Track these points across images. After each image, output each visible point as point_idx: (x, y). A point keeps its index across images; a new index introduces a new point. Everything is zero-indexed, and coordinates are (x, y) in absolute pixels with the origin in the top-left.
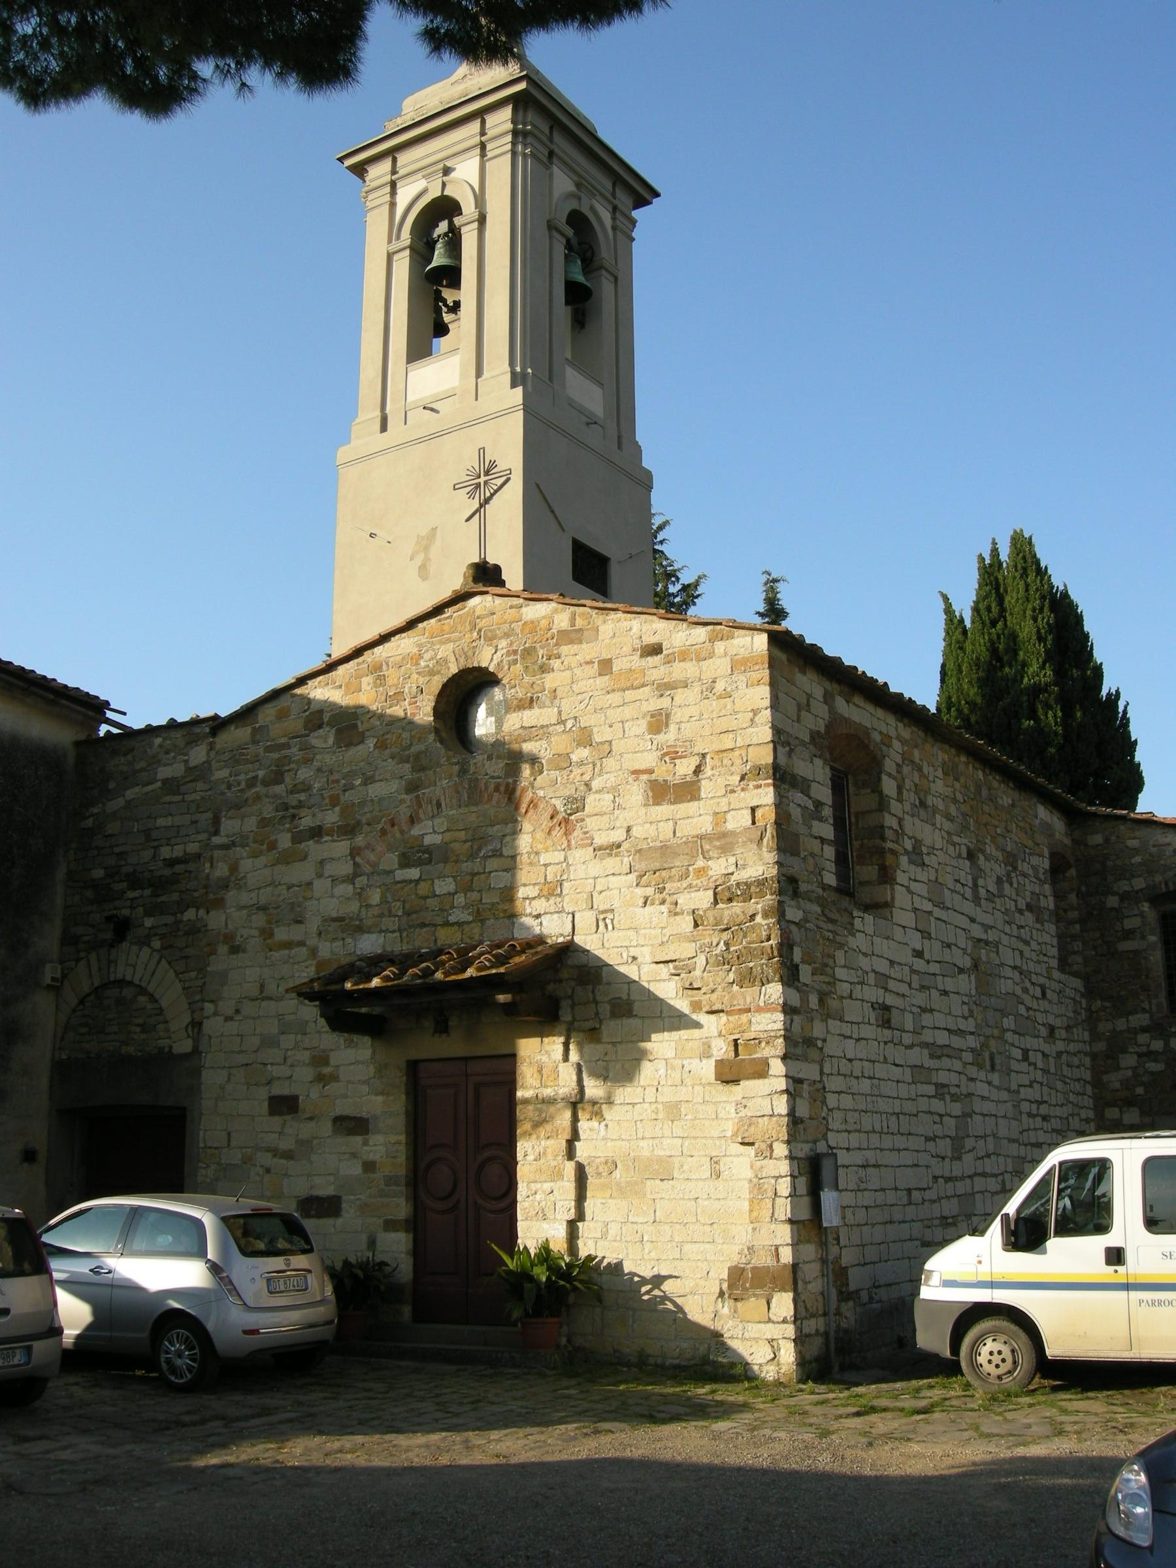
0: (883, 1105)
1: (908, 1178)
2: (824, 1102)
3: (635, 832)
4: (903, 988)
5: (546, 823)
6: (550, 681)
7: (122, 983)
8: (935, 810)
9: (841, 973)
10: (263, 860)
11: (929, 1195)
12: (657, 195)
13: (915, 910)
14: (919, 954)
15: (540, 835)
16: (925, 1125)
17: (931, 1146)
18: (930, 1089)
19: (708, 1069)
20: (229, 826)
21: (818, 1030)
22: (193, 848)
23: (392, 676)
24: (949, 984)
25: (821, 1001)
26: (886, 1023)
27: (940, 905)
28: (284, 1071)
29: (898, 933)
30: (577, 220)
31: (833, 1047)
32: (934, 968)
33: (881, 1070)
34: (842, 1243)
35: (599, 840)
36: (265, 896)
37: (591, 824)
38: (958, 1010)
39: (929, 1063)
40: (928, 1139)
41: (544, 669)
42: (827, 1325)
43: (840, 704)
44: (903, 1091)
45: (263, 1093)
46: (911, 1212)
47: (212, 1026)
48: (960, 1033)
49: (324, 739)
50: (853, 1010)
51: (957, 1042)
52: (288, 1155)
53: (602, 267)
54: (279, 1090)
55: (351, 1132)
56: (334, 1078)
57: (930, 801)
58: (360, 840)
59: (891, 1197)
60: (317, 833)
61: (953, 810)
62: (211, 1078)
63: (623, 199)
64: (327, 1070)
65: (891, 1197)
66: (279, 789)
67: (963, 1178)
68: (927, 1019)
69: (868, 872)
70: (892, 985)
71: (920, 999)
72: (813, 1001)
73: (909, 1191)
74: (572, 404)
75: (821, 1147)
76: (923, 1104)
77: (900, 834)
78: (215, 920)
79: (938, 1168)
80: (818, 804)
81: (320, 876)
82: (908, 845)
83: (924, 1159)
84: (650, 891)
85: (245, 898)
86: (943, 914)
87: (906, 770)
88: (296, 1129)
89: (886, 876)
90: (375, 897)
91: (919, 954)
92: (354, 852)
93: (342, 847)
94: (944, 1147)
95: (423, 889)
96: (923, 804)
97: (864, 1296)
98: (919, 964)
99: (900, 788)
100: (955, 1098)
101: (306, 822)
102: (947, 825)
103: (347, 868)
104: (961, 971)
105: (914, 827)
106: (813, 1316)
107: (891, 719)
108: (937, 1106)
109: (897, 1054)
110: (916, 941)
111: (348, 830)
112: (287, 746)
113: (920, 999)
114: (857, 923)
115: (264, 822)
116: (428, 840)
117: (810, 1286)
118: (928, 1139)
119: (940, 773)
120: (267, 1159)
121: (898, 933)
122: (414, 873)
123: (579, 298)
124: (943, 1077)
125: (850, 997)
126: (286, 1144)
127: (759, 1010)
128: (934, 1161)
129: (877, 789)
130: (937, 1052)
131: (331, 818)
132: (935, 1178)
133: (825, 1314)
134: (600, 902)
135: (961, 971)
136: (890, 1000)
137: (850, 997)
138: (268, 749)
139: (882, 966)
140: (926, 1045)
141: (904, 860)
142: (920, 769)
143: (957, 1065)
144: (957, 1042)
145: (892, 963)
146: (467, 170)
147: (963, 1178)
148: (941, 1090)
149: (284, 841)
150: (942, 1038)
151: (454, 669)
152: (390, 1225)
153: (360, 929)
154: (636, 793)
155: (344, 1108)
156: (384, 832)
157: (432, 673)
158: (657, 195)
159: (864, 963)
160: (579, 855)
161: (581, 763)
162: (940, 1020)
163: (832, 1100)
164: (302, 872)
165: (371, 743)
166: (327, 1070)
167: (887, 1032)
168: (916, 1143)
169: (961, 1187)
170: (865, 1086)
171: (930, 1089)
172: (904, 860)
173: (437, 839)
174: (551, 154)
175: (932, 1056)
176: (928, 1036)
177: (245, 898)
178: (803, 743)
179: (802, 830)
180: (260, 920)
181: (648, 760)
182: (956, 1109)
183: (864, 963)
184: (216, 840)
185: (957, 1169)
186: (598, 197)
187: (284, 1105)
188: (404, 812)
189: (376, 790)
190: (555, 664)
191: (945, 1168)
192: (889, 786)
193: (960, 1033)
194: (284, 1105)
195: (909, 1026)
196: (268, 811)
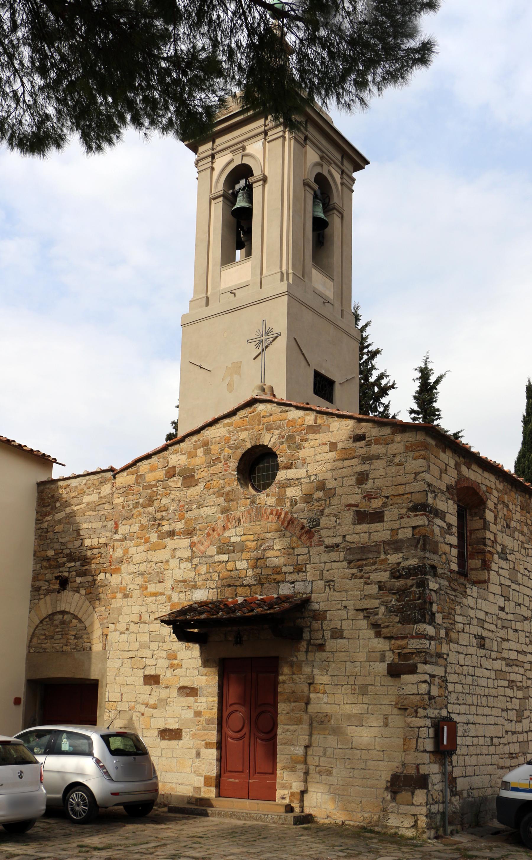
0: (478, 690)
1: (491, 731)
2: (446, 688)
3: (348, 538)
4: (493, 627)
5: (298, 532)
6: (302, 453)
7: (63, 613)
8: (515, 529)
9: (458, 618)
10: (142, 548)
11: (503, 741)
12: (367, 163)
13: (501, 585)
14: (502, 609)
15: (294, 539)
16: (502, 703)
17: (505, 714)
18: (506, 683)
19: (382, 668)
20: (123, 529)
21: (444, 649)
22: (103, 540)
23: (215, 449)
24: (518, 626)
25: (447, 634)
26: (482, 646)
27: (516, 582)
28: (152, 662)
29: (491, 597)
30: (320, 179)
31: (453, 658)
32: (510, 617)
33: (478, 672)
34: (454, 764)
35: (329, 541)
36: (142, 568)
37: (323, 533)
38: (523, 640)
39: (505, 669)
40: (503, 710)
41: (299, 447)
42: (445, 808)
43: (464, 470)
44: (490, 683)
45: (141, 673)
46: (492, 749)
47: (113, 637)
48: (524, 653)
49: (176, 482)
50: (464, 639)
51: (521, 658)
52: (155, 707)
53: (334, 208)
54: (150, 671)
55: (188, 695)
56: (179, 666)
57: (512, 524)
58: (195, 539)
59: (481, 741)
60: (172, 534)
61: (525, 529)
62: (112, 665)
63: (347, 166)
64: (175, 662)
65: (481, 741)
66: (151, 509)
67: (522, 733)
68: (505, 645)
69: (475, 563)
70: (486, 625)
71: (502, 633)
72: (443, 633)
73: (492, 738)
74: (315, 292)
75: (444, 713)
76: (501, 691)
77: (495, 541)
78: (115, 580)
79: (508, 726)
80: (450, 526)
81: (173, 557)
82: (499, 549)
83: (501, 721)
84: (355, 571)
85: (132, 568)
86: (517, 587)
87: (500, 507)
88: (157, 693)
89: (486, 566)
90: (203, 569)
91: (502, 609)
92: (192, 545)
93: (185, 542)
94: (512, 715)
95: (230, 566)
96: (508, 526)
97: (465, 794)
98: (502, 615)
99: (496, 519)
100: (519, 688)
101: (166, 527)
102: (521, 538)
103: (189, 554)
104: (526, 619)
105: (503, 539)
106: (436, 803)
107: (492, 478)
108: (509, 692)
109: (488, 664)
110: (501, 602)
111: (189, 533)
112: (155, 486)
113: (502, 633)
114: (468, 591)
115: (142, 527)
116: (233, 540)
117: (435, 787)
118: (503, 710)
119: (519, 509)
120: (141, 708)
121: (491, 597)
122: (225, 557)
123: (320, 226)
124: (513, 677)
125: (463, 631)
126: (153, 700)
127: (413, 637)
128: (506, 723)
129: (483, 517)
130: (510, 663)
131: (180, 526)
132: (507, 732)
133: (443, 802)
134: (327, 576)
135: (526, 619)
136: (485, 634)
137: (463, 631)
138: (145, 487)
139: (482, 615)
140: (504, 659)
141: (496, 557)
142: (507, 506)
143: (521, 670)
144: (521, 658)
145: (487, 613)
146: (255, 148)
147: (522, 733)
148: (512, 684)
149: (154, 538)
150: (513, 655)
151: (249, 446)
152: (208, 745)
153: (195, 587)
154: (349, 516)
155: (184, 682)
156: (208, 535)
157: (237, 448)
158: (367, 163)
159: (472, 613)
160: (314, 550)
161: (318, 500)
162: (512, 645)
163: (451, 687)
164: (163, 555)
165: (202, 485)
166: (175, 662)
167: (483, 652)
168: (498, 712)
169: (521, 738)
170: (469, 680)
171: (506, 683)
172: (496, 557)
173: (238, 539)
174: (306, 138)
175: (507, 665)
176: (505, 654)
177: (132, 568)
178: (443, 492)
179: (441, 539)
180: (139, 580)
181: (357, 499)
182: (520, 694)
183: (472, 613)
184: (116, 536)
185: (519, 727)
186: (245, 144)
187: (152, 680)
188: (220, 525)
189: (204, 512)
190: (306, 444)
191: (512, 727)
192: (489, 516)
193: (524, 653)
194: (152, 680)
195: (495, 648)
196: (145, 521)
